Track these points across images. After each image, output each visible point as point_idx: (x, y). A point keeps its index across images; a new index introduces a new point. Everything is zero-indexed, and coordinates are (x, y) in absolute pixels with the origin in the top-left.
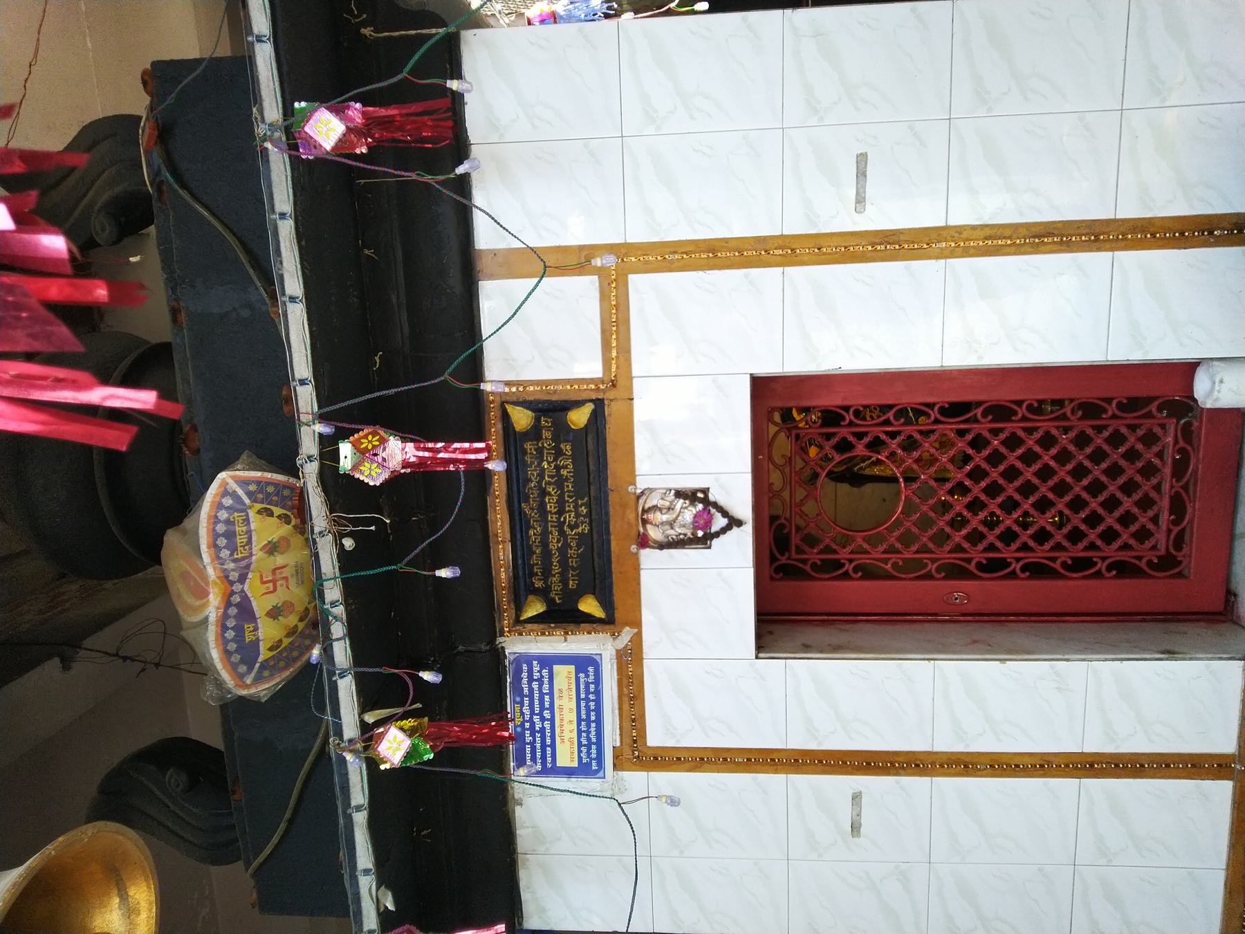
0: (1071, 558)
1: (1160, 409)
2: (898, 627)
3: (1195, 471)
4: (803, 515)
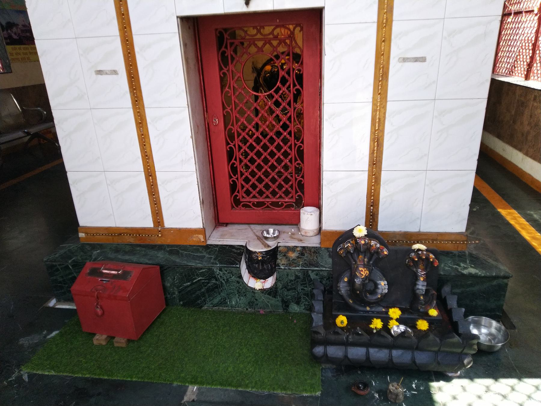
0: (237, 166)
1: (298, 196)
2: (199, 94)
3: (274, 209)
4: (249, 46)
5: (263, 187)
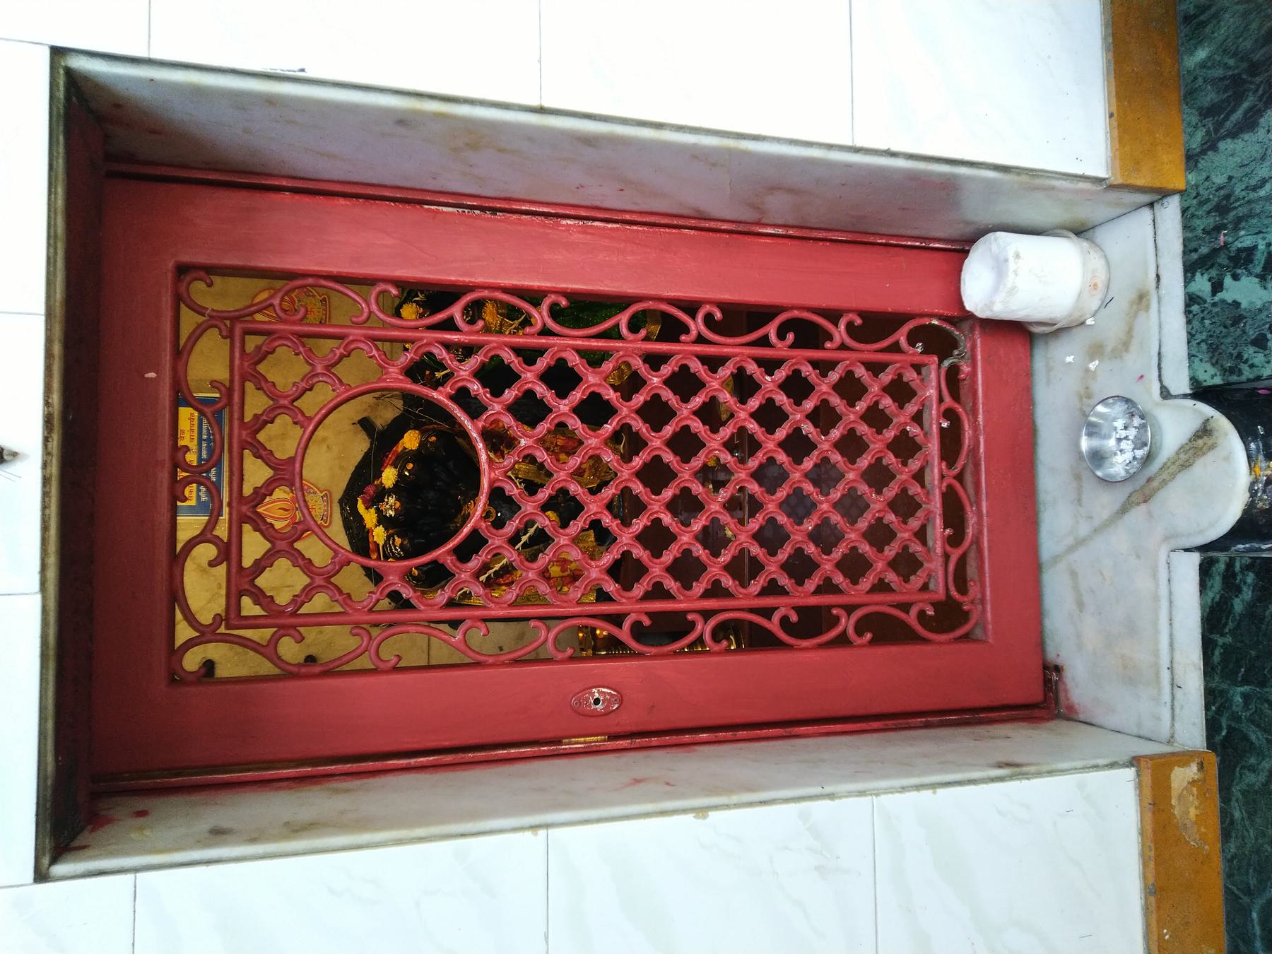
3: (974, 450)
5: (879, 492)
